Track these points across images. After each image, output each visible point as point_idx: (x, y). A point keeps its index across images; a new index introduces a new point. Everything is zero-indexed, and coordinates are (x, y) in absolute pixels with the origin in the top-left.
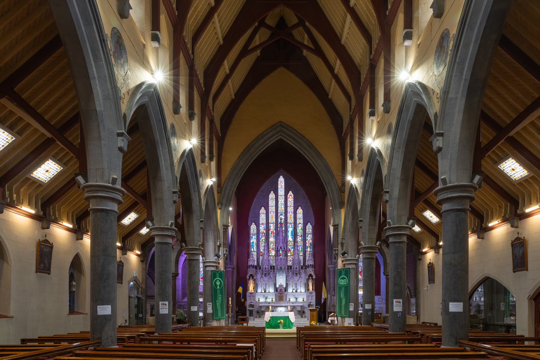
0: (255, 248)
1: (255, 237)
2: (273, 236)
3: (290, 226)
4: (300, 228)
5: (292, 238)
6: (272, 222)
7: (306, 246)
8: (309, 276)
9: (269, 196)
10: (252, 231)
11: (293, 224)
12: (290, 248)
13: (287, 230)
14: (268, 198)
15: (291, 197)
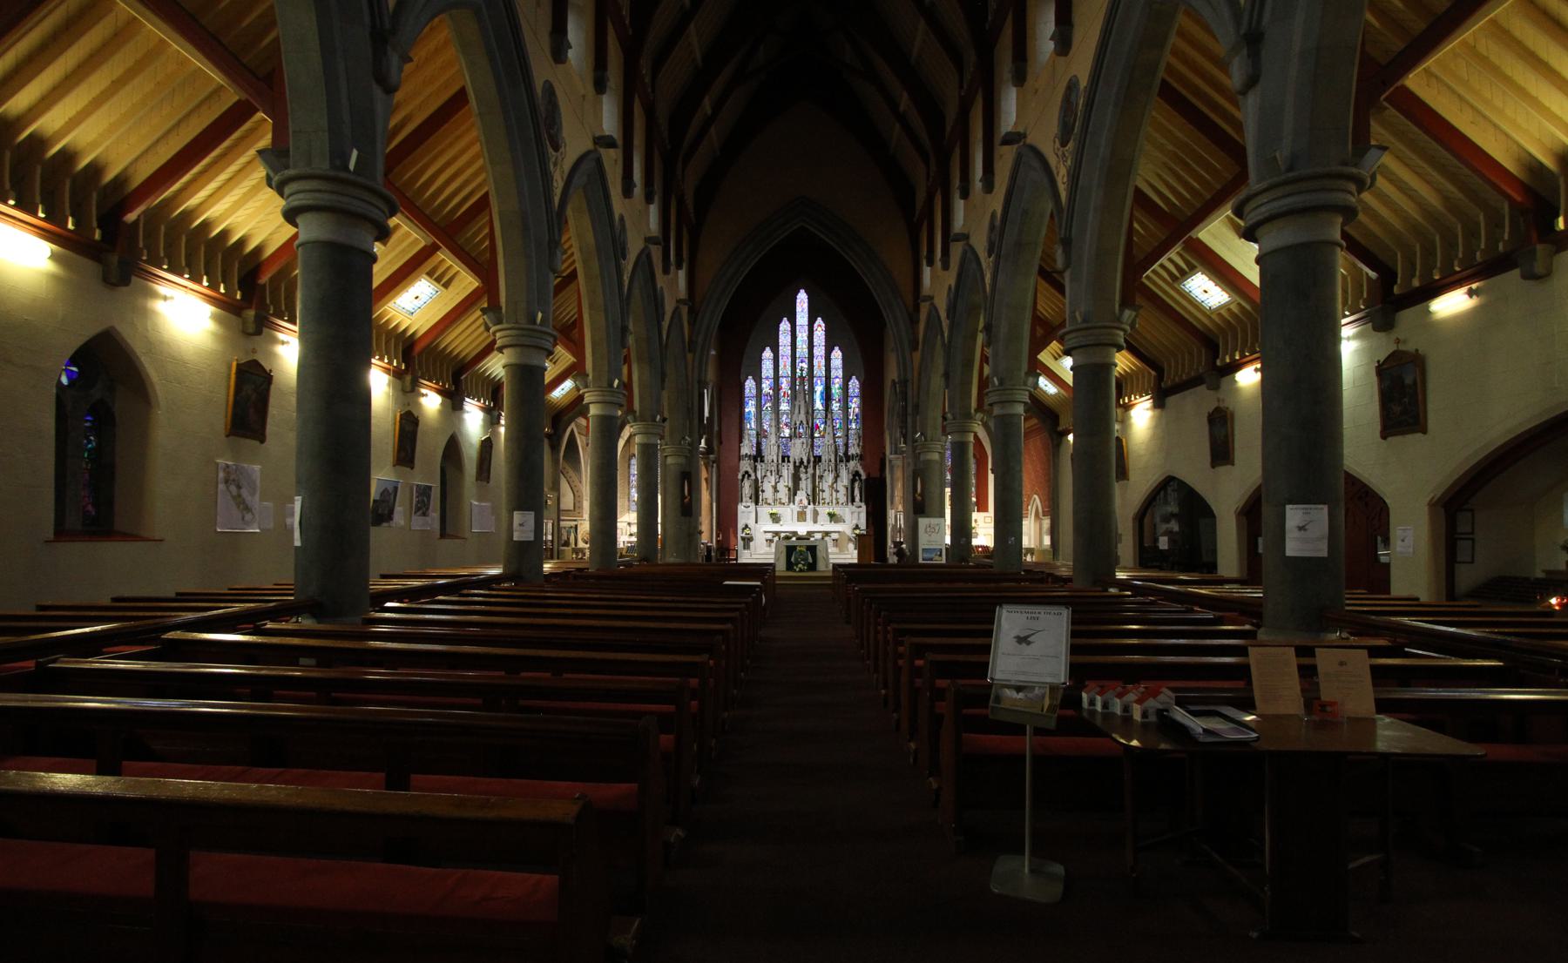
0: (753, 424)
1: (753, 403)
2: (786, 401)
3: (819, 382)
4: (837, 386)
5: (822, 404)
6: (786, 375)
7: (848, 418)
8: (854, 476)
9: (778, 327)
10: (747, 391)
11: (824, 379)
12: (818, 421)
13: (813, 389)
14: (778, 330)
15: (819, 329)
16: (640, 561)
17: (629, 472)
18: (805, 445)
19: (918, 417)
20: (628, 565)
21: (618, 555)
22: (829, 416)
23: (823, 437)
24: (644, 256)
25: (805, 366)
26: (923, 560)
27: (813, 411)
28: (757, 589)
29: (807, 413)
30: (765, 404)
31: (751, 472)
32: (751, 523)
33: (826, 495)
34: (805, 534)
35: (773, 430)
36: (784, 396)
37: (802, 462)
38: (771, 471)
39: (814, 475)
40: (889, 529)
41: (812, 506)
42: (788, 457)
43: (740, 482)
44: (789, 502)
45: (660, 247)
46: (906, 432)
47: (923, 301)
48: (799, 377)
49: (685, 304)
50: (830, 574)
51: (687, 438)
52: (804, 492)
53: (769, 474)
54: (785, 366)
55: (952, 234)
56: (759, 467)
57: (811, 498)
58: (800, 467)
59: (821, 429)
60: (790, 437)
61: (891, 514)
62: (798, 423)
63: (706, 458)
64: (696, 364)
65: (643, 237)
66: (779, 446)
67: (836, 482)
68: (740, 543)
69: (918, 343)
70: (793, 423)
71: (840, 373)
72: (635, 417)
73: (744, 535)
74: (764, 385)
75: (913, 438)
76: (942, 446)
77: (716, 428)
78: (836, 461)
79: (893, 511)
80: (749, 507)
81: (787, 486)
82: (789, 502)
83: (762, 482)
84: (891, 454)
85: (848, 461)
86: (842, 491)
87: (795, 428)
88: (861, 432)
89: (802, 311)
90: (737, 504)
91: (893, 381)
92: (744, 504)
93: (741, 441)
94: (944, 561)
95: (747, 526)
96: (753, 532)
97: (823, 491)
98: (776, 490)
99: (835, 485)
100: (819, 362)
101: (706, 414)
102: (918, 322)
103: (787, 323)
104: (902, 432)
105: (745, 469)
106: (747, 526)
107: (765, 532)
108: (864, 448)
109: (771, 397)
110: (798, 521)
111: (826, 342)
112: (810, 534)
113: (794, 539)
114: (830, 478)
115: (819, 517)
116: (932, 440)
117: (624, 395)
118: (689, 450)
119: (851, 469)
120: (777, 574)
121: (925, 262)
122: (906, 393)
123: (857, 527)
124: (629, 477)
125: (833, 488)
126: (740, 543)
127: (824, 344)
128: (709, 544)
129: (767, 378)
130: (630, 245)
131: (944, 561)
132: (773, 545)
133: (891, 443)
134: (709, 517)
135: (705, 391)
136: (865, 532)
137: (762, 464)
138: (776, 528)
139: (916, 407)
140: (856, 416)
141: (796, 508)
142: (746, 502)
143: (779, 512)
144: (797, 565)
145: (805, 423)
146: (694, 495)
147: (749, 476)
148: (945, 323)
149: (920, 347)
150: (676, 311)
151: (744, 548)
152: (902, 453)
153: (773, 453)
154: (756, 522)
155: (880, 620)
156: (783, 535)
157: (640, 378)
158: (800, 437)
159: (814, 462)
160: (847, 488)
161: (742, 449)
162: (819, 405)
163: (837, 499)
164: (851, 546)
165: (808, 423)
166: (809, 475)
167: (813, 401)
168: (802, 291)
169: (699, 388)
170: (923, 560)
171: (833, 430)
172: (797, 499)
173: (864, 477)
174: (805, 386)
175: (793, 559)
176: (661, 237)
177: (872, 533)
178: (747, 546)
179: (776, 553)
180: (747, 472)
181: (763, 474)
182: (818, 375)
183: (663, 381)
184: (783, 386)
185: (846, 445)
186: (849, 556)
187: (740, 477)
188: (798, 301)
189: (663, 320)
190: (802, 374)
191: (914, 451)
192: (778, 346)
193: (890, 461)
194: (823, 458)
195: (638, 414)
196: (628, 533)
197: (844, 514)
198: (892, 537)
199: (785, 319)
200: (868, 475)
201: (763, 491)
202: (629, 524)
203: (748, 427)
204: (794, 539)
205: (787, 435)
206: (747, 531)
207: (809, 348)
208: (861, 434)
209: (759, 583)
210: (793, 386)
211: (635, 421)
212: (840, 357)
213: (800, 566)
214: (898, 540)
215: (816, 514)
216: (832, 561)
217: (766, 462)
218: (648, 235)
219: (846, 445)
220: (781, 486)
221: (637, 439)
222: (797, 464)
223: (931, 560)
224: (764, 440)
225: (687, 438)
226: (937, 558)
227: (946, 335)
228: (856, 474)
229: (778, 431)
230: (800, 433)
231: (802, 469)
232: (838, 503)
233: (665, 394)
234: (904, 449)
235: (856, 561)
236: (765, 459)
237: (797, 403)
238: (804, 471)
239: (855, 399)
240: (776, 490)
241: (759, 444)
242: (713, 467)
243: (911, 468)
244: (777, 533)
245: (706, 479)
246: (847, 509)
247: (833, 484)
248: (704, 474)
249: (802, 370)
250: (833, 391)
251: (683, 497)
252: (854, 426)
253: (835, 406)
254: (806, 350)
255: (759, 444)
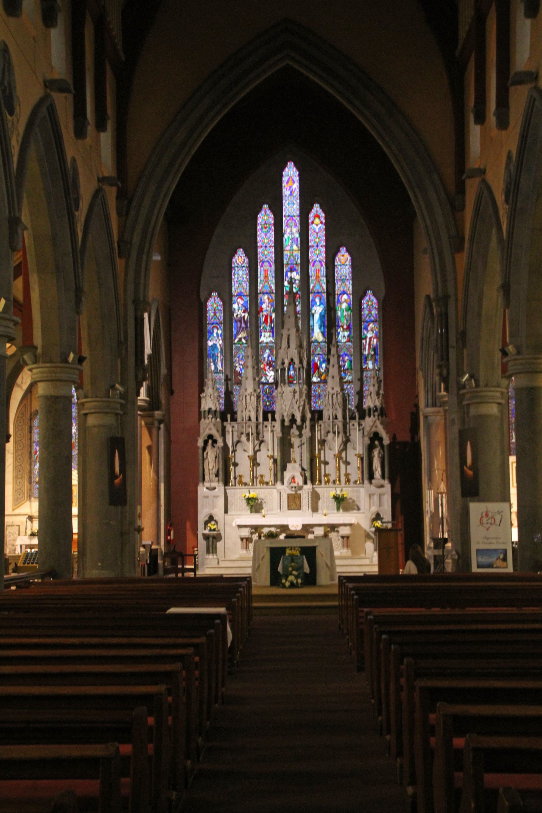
0: (219, 364)
1: (220, 332)
2: (268, 328)
3: (317, 300)
4: (344, 306)
5: (323, 333)
6: (268, 290)
7: (361, 354)
8: (372, 440)
9: (256, 219)
10: (210, 314)
11: (325, 295)
12: (316, 359)
14: (255, 225)
15: (317, 221)
16: (43, 577)
17: (31, 439)
18: (297, 396)
19: (465, 351)
20: (23, 584)
21: (11, 567)
22: (333, 351)
23: (325, 382)
24: (44, 111)
25: (296, 276)
26: (479, 566)
27: (309, 343)
28: (218, 621)
29: (300, 346)
30: (238, 333)
31: (217, 436)
32: (218, 512)
33: (331, 469)
34: (299, 528)
35: (250, 372)
36: (266, 321)
37: (293, 420)
38: (248, 435)
39: (312, 439)
40: (427, 519)
41: (309, 486)
42: (273, 413)
43: (200, 451)
44: (276, 480)
45: (70, 97)
46: (448, 373)
47: (469, 177)
48: (287, 293)
49: (111, 185)
50: (336, 591)
51: (117, 386)
52: (297, 466)
53: (244, 438)
54: (266, 277)
55: (512, 74)
56: (229, 428)
57: (308, 474)
58: (291, 427)
59: (322, 370)
60: (276, 383)
61: (428, 496)
62: (287, 362)
63: (148, 416)
64: (131, 274)
65: (41, 80)
66: (258, 397)
67: (345, 449)
68: (202, 543)
69: (463, 239)
70: (279, 362)
71: (349, 286)
72: (35, 356)
73: (207, 532)
74: (235, 306)
75: (458, 383)
76: (502, 393)
77: (164, 371)
78: (344, 417)
79: (432, 492)
80: (215, 488)
81: (272, 457)
82: (276, 480)
83: (234, 451)
84: (427, 406)
85: (362, 417)
86: (355, 462)
87: (283, 370)
88: (381, 373)
89: (291, 194)
90: (196, 485)
91: (428, 297)
92: (207, 484)
93: (201, 390)
94: (510, 569)
95: (211, 518)
96: (221, 527)
97: (326, 463)
98: (254, 462)
99: (343, 455)
100: (318, 271)
101: (148, 350)
102: (463, 208)
103: (269, 212)
104: (441, 374)
105: (207, 432)
106: (211, 518)
107: (240, 526)
108: (385, 397)
109: (246, 323)
110: (289, 508)
111: (327, 240)
112: (307, 528)
113: (282, 537)
114: (335, 443)
115: (320, 503)
116: (486, 386)
117: (16, 324)
118: (122, 404)
119: (367, 429)
120: (254, 592)
121: (471, 118)
122: (447, 315)
123: (378, 517)
124: (31, 446)
125: (340, 458)
126: (202, 543)
127: (323, 243)
128: (154, 547)
129: (240, 295)
130: (19, 91)
131: (510, 569)
132: (251, 546)
133: (427, 392)
134: (154, 505)
135: (146, 315)
136: (390, 526)
137: (234, 423)
138: (256, 520)
139: (463, 335)
140: (375, 349)
141: (285, 489)
142: (210, 481)
143: (260, 497)
144: (286, 578)
145: (297, 361)
146: (129, 473)
147: (215, 442)
148: (503, 210)
149: (467, 245)
150: (98, 194)
151: (208, 552)
152: (443, 404)
153: (250, 407)
154: (226, 511)
155: (402, 667)
156: (266, 531)
157: (41, 295)
158: (290, 383)
159: (312, 419)
160: (362, 459)
161: (203, 402)
162: (317, 334)
163: (347, 475)
164: (370, 546)
165: (301, 362)
166: (305, 439)
167: (309, 330)
168: (291, 165)
169: (136, 310)
170: (479, 566)
171: (340, 372)
172: (287, 475)
173: (386, 441)
174: (296, 306)
175: (280, 569)
176: (70, 82)
177: (400, 526)
178: (211, 549)
179: (254, 559)
180: (210, 437)
181: (236, 439)
182: (315, 290)
183: (78, 301)
184: (264, 306)
185: (360, 394)
186: (367, 562)
187: (200, 443)
188: (285, 179)
189: (77, 208)
190: (291, 288)
191: (460, 403)
192: (256, 248)
193: (426, 417)
194: (325, 414)
195: (39, 350)
196: (29, 532)
197: (358, 497)
198: (432, 532)
199: (266, 206)
200: (393, 438)
201: (236, 465)
202: (31, 518)
203: (213, 368)
204: (282, 537)
205: (271, 380)
206: (212, 525)
207: (276, 253)
208: (382, 378)
209: (222, 610)
210: (278, 306)
211: (35, 362)
212: (348, 263)
213: (291, 578)
214: (440, 536)
215: (315, 497)
216: (338, 570)
217: (239, 420)
218: (49, 77)
219: (360, 394)
220: (262, 457)
221: (41, 389)
222: (287, 423)
223: (491, 566)
224: (236, 387)
225: (117, 386)
226: (500, 563)
227: (504, 227)
228: (376, 437)
229: (258, 375)
230: (290, 377)
231: (294, 431)
232: (348, 481)
233: (84, 320)
234: (446, 399)
235: (374, 570)
236: (239, 417)
237: (285, 332)
238: (297, 433)
239: (371, 325)
240: (254, 462)
241: (229, 394)
242: (159, 428)
243: (456, 429)
244: (256, 528)
245: (149, 448)
246: (362, 490)
247: (340, 452)
248: (145, 440)
249: (291, 283)
250: (339, 314)
251: (112, 476)
252: (370, 365)
253: (343, 336)
254: (297, 253)
255: (229, 394)
